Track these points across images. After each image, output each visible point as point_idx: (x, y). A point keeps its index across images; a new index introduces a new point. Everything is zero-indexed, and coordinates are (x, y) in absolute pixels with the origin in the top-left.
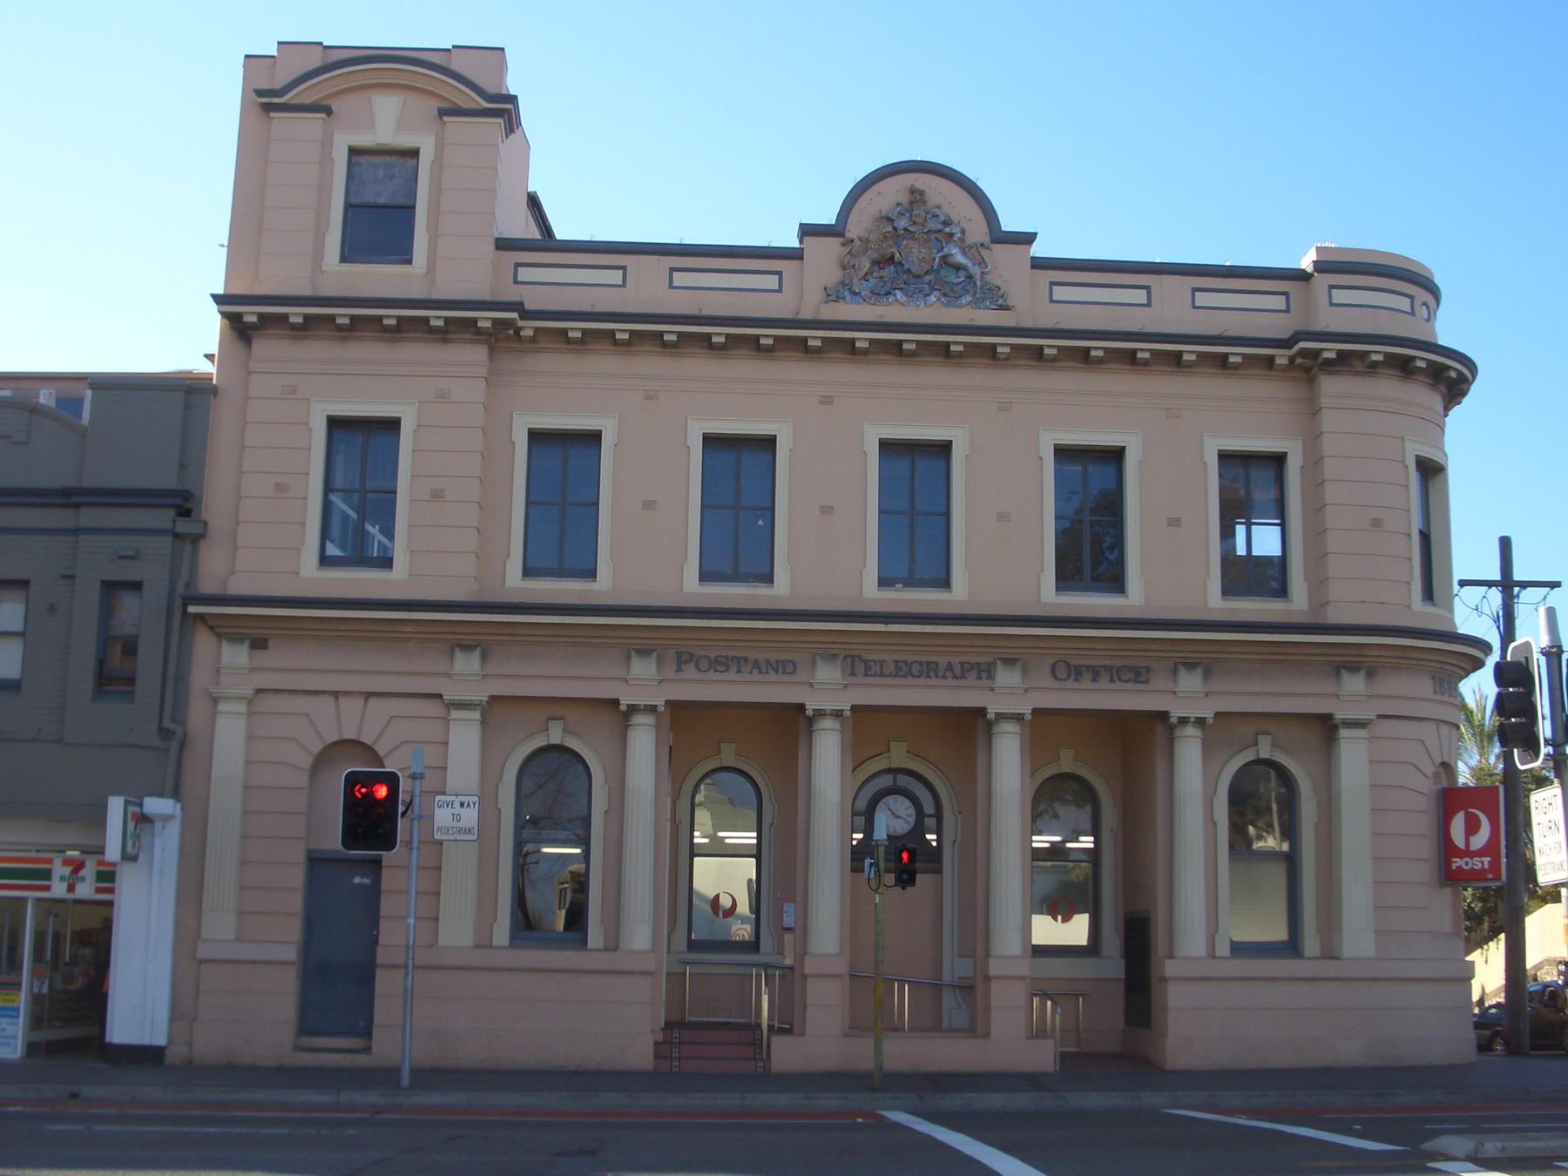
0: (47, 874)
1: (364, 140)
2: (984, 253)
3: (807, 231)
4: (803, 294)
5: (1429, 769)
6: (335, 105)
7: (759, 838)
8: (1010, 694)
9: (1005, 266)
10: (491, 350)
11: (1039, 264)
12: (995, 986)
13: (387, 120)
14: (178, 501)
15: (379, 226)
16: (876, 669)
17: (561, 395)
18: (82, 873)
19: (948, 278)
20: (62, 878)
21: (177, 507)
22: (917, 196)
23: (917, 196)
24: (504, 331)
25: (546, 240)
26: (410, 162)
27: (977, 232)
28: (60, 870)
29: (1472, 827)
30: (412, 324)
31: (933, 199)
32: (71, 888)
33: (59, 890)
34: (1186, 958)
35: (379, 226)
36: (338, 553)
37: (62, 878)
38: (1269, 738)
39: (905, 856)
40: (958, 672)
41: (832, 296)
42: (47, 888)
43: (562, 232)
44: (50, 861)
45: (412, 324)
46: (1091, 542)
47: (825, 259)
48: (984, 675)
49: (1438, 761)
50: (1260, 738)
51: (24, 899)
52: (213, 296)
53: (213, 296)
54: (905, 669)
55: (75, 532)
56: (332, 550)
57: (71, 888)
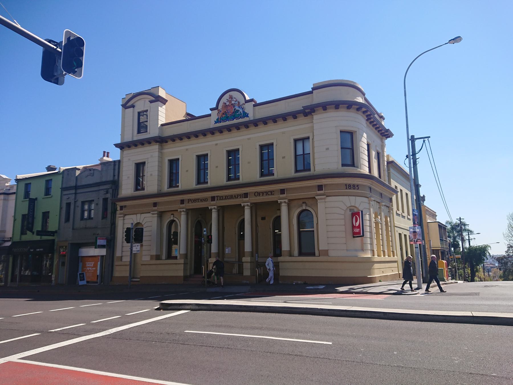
1: (139, 110)
3: (212, 109)
4: (211, 123)
6: (134, 104)
8: (213, 206)
9: (249, 108)
12: (244, 264)
15: (142, 127)
17: (172, 151)
19: (235, 115)
22: (231, 97)
23: (231, 97)
24: (161, 140)
26: (64, 186)
27: (242, 101)
30: (149, 141)
31: (234, 96)
34: (13, 235)
35: (142, 127)
45: (149, 141)
47: (215, 116)
55: (99, 190)
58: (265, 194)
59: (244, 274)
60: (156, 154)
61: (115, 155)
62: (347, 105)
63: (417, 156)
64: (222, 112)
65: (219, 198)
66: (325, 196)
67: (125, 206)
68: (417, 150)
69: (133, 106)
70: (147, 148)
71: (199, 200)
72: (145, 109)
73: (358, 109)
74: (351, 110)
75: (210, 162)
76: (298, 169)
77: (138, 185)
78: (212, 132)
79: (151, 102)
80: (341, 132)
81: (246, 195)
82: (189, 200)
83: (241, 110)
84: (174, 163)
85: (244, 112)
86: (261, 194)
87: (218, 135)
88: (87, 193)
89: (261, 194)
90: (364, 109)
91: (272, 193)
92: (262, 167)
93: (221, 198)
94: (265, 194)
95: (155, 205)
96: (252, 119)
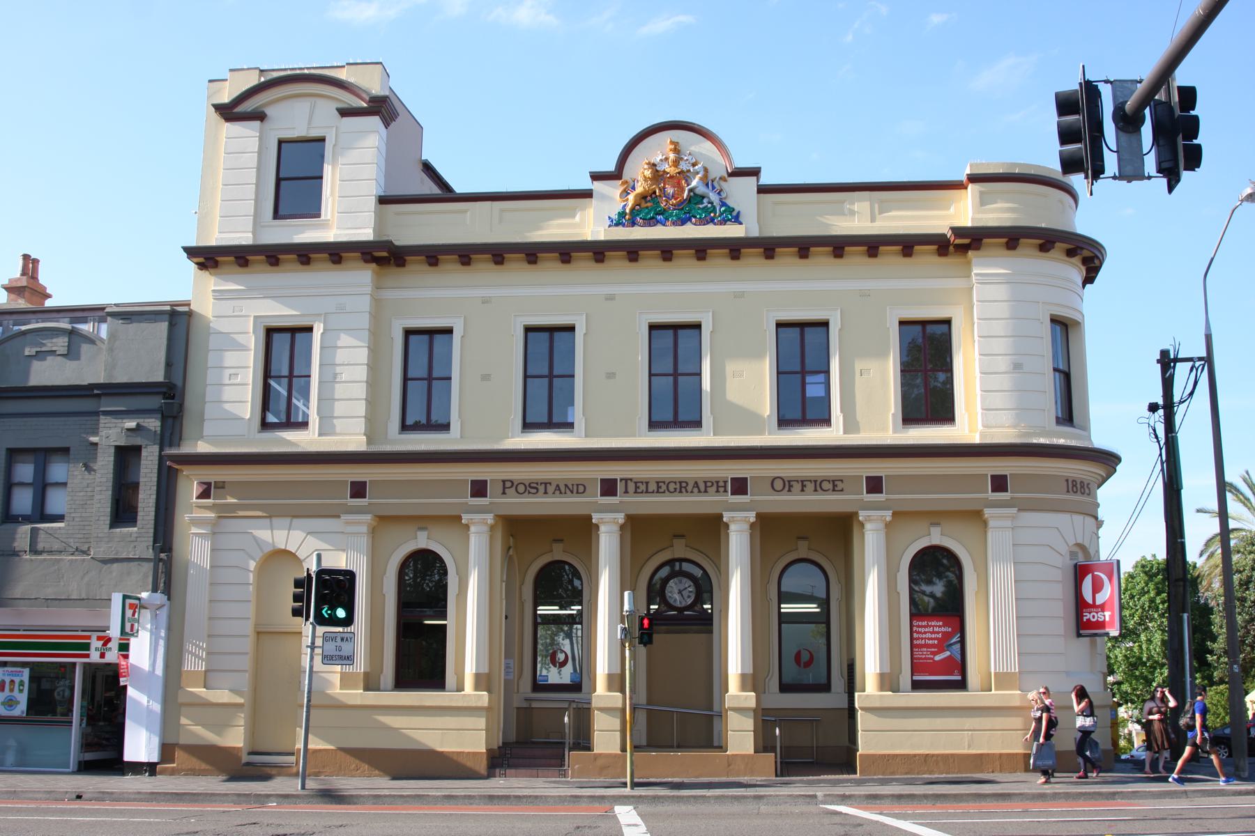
0: (87, 647)
2: (722, 183)
3: (596, 177)
5: (1064, 550)
6: (268, 111)
7: (780, 608)
9: (741, 194)
10: (377, 275)
11: (763, 190)
13: (295, 117)
14: (164, 390)
16: (643, 487)
17: (430, 298)
18: (109, 645)
20: (97, 649)
21: (164, 393)
25: (446, 194)
28: (96, 644)
29: (1097, 587)
32: (103, 655)
33: (95, 657)
36: (276, 420)
37: (97, 649)
38: (683, 541)
39: (646, 622)
40: (702, 489)
41: (622, 220)
42: (87, 656)
43: (459, 188)
44: (89, 637)
46: (675, 398)
47: (612, 199)
48: (721, 489)
49: (1071, 542)
50: (676, 541)
51: (74, 664)
52: (186, 249)
53: (186, 249)
54: (664, 487)
56: (271, 418)
57: (103, 655)
58: (810, 487)
59: (598, 749)
60: (364, 303)
61: (181, 283)
62: (1004, 240)
63: (1179, 412)
64: (639, 189)
65: (631, 486)
66: (1014, 510)
67: (221, 486)
68: (1176, 399)
69: (259, 116)
70: (323, 277)
71: (551, 489)
72: (314, 133)
73: (1070, 253)
74: (1052, 253)
75: (461, 360)
76: (409, 422)
77: (277, 408)
78: (598, 251)
79: (345, 113)
80: (901, 323)
81: (740, 486)
82: (507, 486)
83: (713, 197)
84: (427, 342)
85: (723, 204)
86: (797, 487)
87: (617, 269)
88: (34, 420)
89: (797, 487)
90: (1086, 253)
91: (835, 485)
92: (265, 407)
93: (641, 487)
94: (810, 487)
95: (358, 490)
96: (755, 233)
